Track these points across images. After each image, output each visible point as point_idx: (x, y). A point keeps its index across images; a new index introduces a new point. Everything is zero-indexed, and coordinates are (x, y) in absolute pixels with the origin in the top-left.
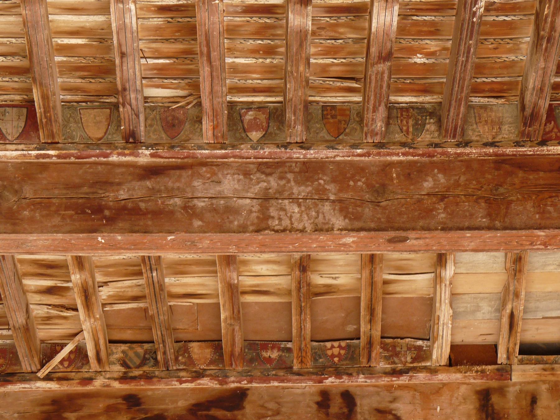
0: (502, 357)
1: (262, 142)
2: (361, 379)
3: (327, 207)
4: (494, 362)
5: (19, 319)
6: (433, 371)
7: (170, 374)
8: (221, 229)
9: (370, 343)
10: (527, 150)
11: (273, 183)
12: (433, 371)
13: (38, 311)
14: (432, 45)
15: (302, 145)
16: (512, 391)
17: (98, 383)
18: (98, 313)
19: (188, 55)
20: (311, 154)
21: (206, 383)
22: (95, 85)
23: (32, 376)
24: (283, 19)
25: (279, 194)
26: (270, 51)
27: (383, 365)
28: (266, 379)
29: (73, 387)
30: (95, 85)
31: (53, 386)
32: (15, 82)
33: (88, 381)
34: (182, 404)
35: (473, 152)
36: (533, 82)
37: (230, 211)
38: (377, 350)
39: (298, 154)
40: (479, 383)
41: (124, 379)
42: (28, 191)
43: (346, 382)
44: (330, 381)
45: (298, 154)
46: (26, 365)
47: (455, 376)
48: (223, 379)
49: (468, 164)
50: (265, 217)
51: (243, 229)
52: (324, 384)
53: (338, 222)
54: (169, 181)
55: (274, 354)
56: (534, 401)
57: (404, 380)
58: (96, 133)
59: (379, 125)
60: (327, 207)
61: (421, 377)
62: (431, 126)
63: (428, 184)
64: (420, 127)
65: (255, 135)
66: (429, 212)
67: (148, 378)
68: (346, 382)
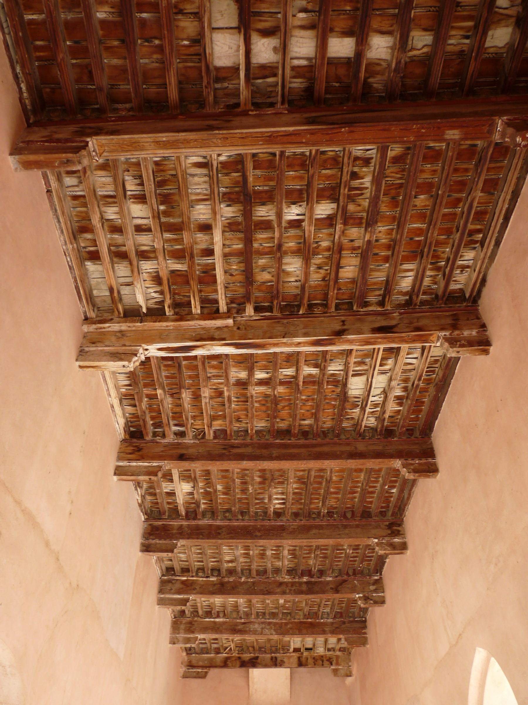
0: (302, 651)
1: (262, 618)
2: (278, 654)
3: (272, 630)
4: (300, 651)
5: (221, 644)
6: (290, 653)
7: (246, 653)
8: (255, 634)
9: (280, 648)
10: (305, 620)
11: (264, 626)
12: (290, 653)
13: (224, 642)
14: (289, 604)
15: (268, 619)
16: (304, 657)
17: (234, 655)
18: (234, 643)
19: (250, 604)
20: (270, 621)
21: (252, 655)
22: (235, 609)
23: (222, 653)
24: (278, 476)
25: (265, 628)
26: (263, 604)
27: (282, 652)
28: (262, 654)
29: (229, 655)
30: (235, 609)
31: (226, 655)
32: (222, 608)
33: (232, 654)
34: (248, 659)
35: (296, 620)
36: (305, 610)
37: (256, 631)
38: (281, 649)
39: (268, 621)
40: (298, 655)
41: (238, 654)
42: (224, 627)
43: (275, 655)
44: (273, 655)
45: (268, 621)
46: (222, 651)
47: (294, 654)
48: (254, 654)
49: (295, 623)
50: (262, 632)
51: (258, 634)
52: (327, 156)
53: (274, 633)
54: (247, 625)
55: (263, 649)
56: (307, 659)
57: (285, 655)
58: (235, 616)
59: (281, 616)
60: (272, 630)
61: (288, 654)
62: (289, 616)
63: (289, 626)
64: (287, 616)
65: (261, 617)
66: (289, 631)
67: (242, 654)
68: (275, 655)
